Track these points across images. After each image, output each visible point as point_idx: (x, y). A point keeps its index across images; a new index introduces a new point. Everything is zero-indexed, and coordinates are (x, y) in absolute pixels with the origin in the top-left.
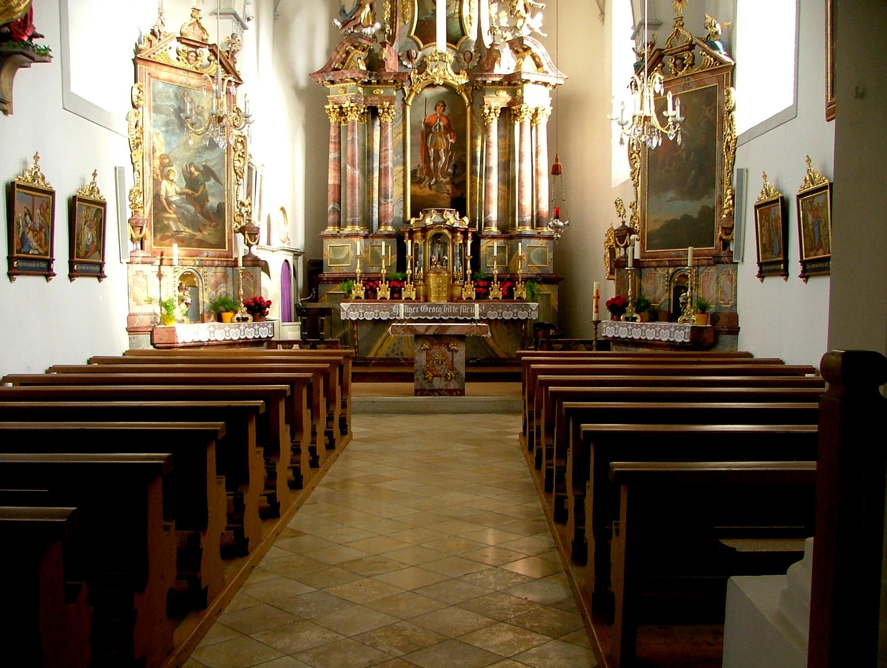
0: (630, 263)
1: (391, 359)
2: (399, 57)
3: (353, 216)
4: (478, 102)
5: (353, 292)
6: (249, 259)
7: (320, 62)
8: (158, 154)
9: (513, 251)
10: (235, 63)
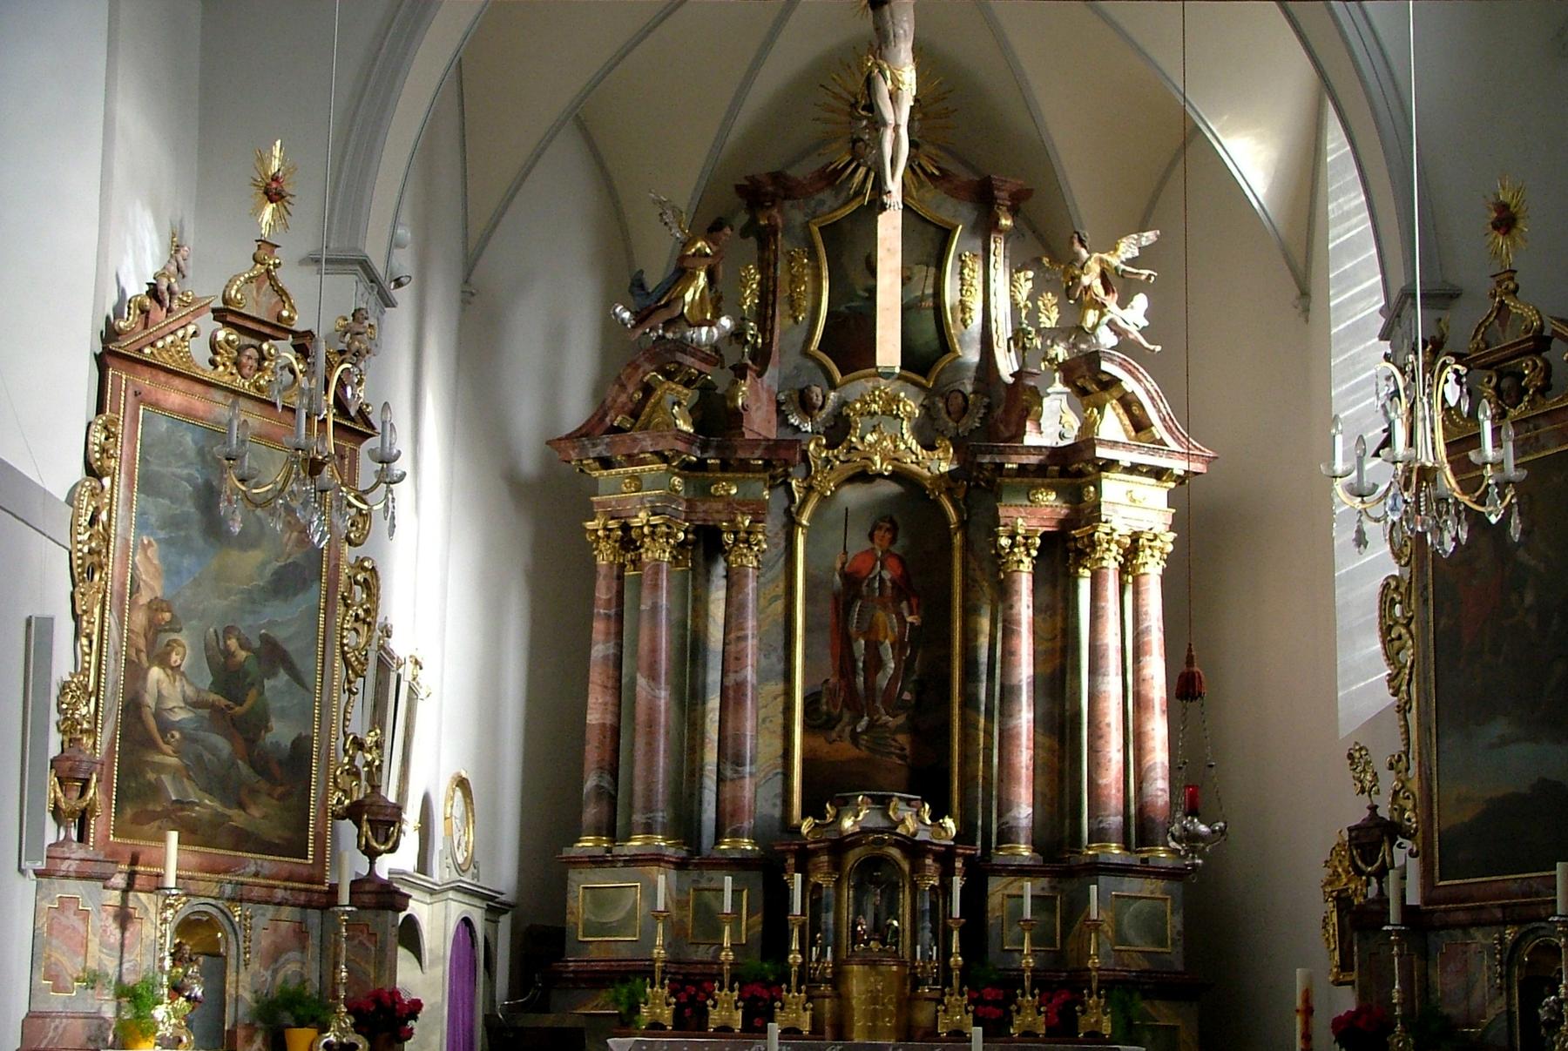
0: (1394, 914)
2: (779, 404)
3: (649, 808)
4: (980, 522)
5: (644, 1010)
6: (368, 887)
7: (575, 412)
8: (144, 598)
9: (1077, 905)
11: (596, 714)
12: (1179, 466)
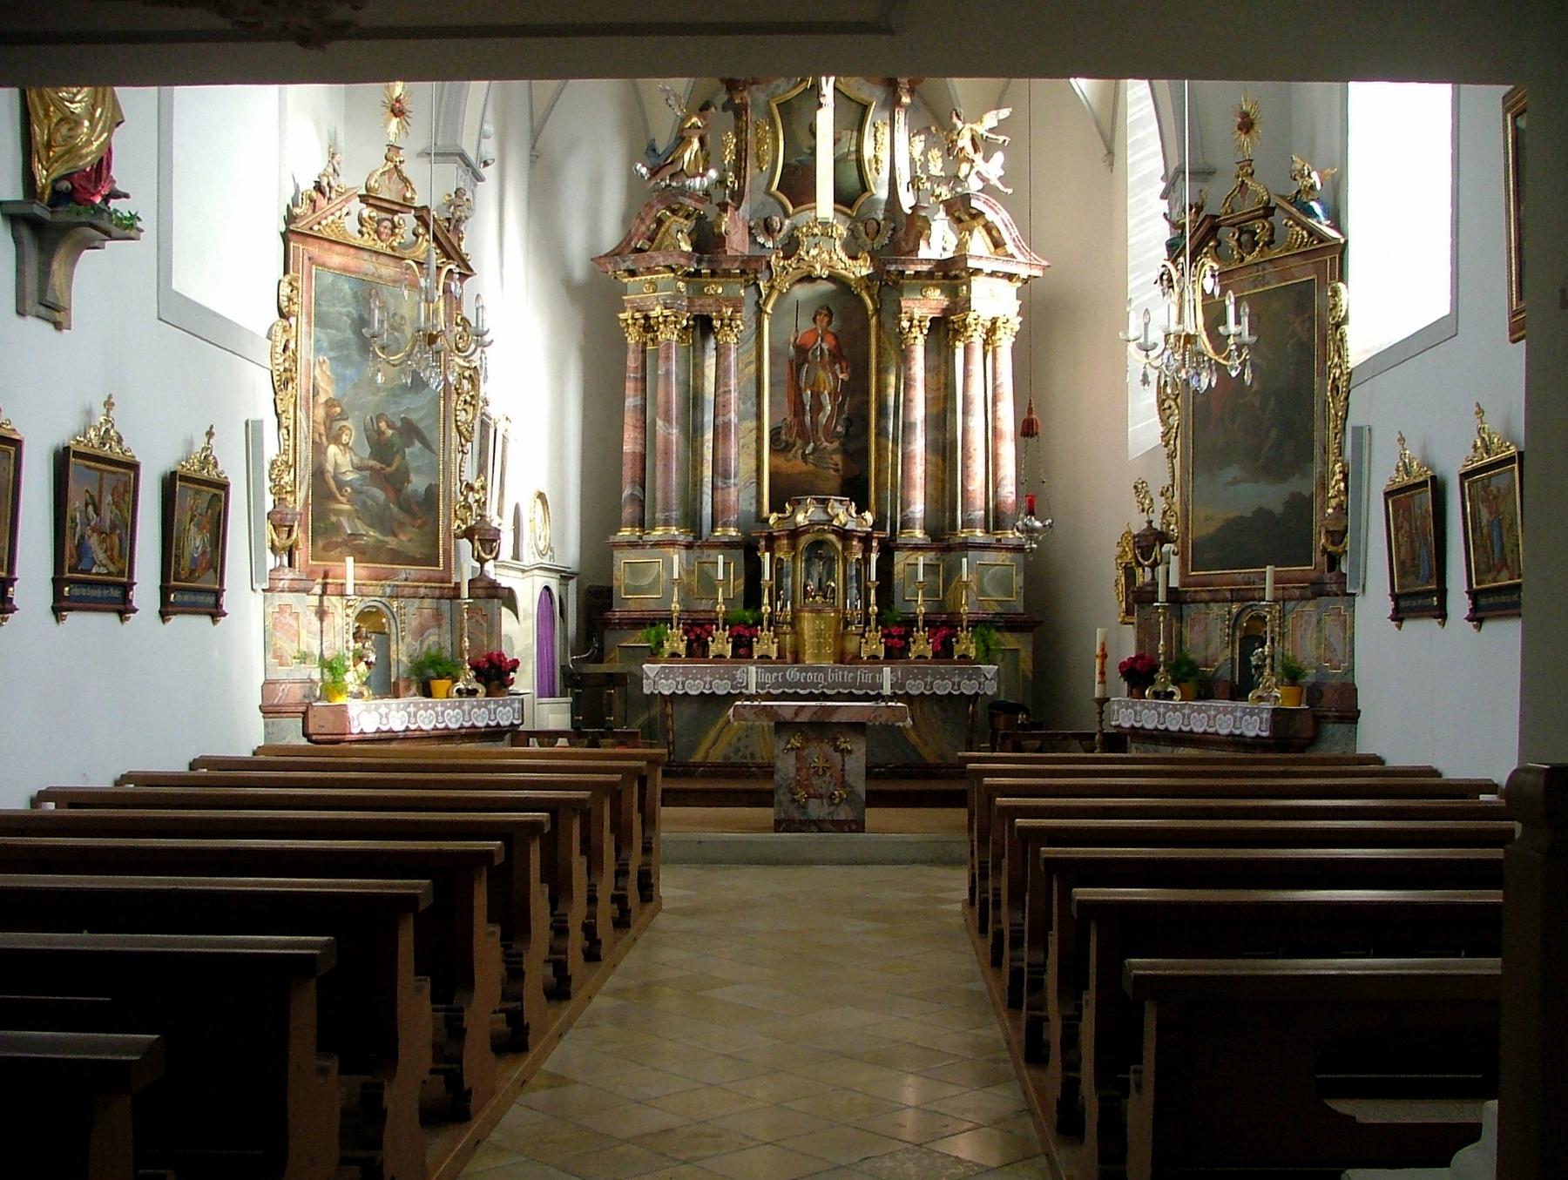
0: (1161, 595)
1: (733, 765)
2: (750, 229)
3: (666, 509)
4: (889, 309)
5: (666, 645)
6: (480, 584)
7: (610, 236)
8: (322, 399)
9: (952, 572)
10: (460, 239)
11: (629, 446)
12: (1024, 272)
